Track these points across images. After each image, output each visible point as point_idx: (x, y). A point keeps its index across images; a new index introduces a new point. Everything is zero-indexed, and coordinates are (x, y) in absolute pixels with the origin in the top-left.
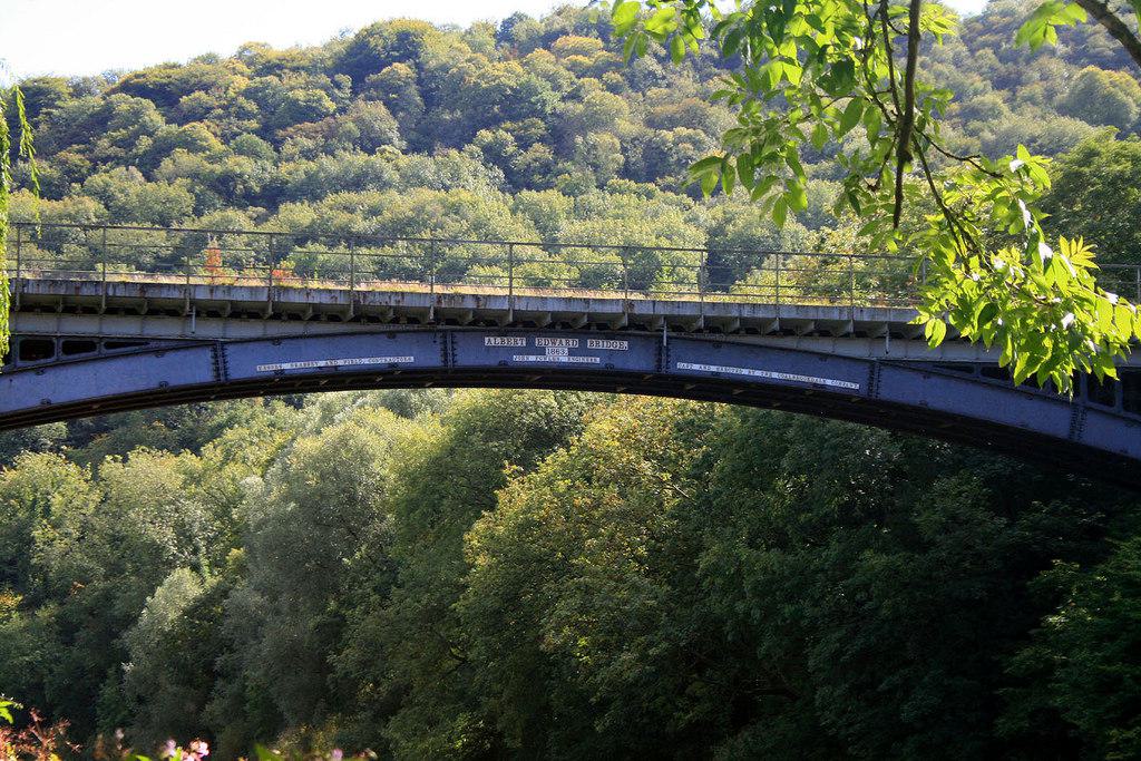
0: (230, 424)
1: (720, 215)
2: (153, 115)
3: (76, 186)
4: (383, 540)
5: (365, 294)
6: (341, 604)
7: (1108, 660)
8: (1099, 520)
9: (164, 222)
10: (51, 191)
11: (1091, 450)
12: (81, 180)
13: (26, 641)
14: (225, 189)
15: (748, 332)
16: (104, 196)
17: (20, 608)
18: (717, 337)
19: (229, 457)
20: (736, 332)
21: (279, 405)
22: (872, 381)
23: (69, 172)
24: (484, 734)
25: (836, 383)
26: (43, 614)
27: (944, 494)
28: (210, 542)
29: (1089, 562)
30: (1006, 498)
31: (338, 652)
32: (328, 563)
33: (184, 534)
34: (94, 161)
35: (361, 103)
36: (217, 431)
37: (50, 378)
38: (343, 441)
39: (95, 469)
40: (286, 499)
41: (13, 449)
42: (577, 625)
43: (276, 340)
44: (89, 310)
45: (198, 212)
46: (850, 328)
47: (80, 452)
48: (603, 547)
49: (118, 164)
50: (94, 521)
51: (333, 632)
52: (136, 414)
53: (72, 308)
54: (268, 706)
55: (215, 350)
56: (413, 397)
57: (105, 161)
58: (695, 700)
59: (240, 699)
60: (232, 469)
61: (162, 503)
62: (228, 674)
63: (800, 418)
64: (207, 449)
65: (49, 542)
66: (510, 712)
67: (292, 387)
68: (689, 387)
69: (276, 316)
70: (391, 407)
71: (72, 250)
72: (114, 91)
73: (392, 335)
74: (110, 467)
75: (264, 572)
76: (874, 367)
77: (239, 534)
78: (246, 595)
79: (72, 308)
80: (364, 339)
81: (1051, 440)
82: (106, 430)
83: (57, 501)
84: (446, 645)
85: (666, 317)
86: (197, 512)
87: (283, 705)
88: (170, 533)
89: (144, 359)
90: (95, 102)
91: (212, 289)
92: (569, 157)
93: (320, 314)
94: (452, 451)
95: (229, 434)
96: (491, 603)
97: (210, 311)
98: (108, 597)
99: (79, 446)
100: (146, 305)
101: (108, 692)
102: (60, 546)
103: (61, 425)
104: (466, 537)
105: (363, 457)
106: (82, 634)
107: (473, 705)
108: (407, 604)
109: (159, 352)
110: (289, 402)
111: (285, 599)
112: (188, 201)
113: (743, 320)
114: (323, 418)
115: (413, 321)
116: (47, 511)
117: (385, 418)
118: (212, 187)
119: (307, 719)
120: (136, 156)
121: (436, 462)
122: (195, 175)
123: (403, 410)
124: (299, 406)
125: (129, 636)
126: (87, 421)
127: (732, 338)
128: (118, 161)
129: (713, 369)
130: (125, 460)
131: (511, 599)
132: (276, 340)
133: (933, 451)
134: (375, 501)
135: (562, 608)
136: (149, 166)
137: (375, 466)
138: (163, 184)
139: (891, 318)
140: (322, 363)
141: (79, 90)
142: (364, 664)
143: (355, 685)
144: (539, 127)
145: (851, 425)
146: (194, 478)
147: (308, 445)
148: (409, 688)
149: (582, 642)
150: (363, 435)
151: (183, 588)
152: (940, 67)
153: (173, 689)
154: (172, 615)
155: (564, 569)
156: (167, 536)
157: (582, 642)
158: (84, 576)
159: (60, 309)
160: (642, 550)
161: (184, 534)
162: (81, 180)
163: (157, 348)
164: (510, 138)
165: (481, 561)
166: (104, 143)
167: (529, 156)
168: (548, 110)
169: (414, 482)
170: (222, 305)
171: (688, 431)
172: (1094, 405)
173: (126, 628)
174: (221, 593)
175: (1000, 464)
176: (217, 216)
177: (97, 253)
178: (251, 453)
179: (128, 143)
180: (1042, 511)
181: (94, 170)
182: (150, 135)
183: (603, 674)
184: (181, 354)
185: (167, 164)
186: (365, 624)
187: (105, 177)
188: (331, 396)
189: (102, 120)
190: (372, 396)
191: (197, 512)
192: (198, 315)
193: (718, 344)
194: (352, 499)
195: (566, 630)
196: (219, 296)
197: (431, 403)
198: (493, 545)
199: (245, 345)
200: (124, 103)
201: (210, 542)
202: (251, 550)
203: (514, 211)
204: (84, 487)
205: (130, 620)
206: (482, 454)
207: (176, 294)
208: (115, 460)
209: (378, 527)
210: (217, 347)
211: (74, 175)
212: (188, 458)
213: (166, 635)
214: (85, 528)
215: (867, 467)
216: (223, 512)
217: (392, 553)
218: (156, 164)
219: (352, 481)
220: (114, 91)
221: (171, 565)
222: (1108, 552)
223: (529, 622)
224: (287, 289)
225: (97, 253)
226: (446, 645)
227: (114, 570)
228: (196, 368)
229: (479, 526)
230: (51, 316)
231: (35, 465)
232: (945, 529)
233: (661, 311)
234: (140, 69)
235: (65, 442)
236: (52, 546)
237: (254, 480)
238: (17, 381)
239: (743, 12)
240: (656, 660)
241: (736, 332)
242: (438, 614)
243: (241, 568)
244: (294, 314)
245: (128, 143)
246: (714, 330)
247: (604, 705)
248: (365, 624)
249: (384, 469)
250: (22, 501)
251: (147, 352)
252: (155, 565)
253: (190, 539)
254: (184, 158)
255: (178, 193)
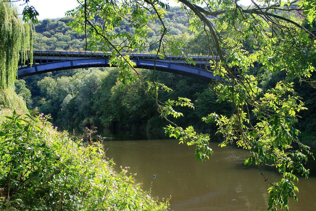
0: (77, 72)
1: (152, 40)
2: (64, 24)
3: (53, 36)
4: (99, 90)
5: (93, 53)
6: (93, 100)
7: (203, 107)
8: (203, 86)
9: (66, 41)
10: (48, 36)
11: (171, 69)
12: (54, 35)
13: (46, 105)
14: (76, 36)
15: (155, 59)
16: (57, 37)
17: (45, 100)
18: (146, 59)
19: (76, 77)
20: (149, 59)
21: (84, 70)
22: (169, 66)
23: (52, 33)
24: (114, 119)
25: (164, 66)
26: (49, 101)
27: (180, 83)
28: (74, 90)
29: (201, 92)
30: (190, 83)
31: (92, 107)
32: (91, 93)
33: (70, 89)
34: (55, 32)
35: (97, 23)
36: (75, 73)
37: (46, 65)
38: (93, 75)
39: (56, 79)
40: (85, 84)
41: (44, 76)
42: (127, 102)
43: (80, 60)
44: (52, 55)
45: (72, 40)
46: (198, 59)
47: (54, 77)
48: (131, 91)
49: (59, 32)
50: (56, 87)
51: (92, 104)
52: (62, 71)
53: (49, 55)
54: (82, 115)
55: (71, 62)
56: (104, 68)
57: (57, 32)
58: (145, 113)
59: (78, 114)
60: (77, 79)
61: (66, 85)
62: (77, 110)
63: (159, 71)
64: (73, 76)
65: (50, 90)
66: (118, 115)
67: (86, 67)
68: (142, 67)
69: (80, 56)
70: (100, 70)
71: (52, 46)
72: (58, 21)
73: (97, 59)
74: (58, 79)
75: (81, 95)
76: (170, 64)
77: (78, 88)
78: (79, 98)
79: (49, 55)
80: (93, 60)
81: (196, 75)
82: (58, 73)
83: (50, 84)
84: (108, 105)
85: (139, 56)
86: (72, 86)
87: (85, 115)
88: (68, 89)
89: (60, 63)
90: (56, 22)
91: (70, 52)
92: (129, 31)
93: (88, 56)
94: (109, 77)
95: (76, 74)
96: (115, 99)
97: (70, 56)
98: (59, 99)
99: (54, 76)
100: (60, 55)
101: (59, 113)
102: (51, 91)
103: (51, 72)
104: (111, 89)
105: (96, 77)
106: (55, 104)
107: (113, 115)
108: (103, 99)
109: (63, 62)
110: (86, 69)
111: (85, 99)
112: (70, 38)
113: (150, 57)
114: (90, 72)
115: (101, 57)
116: (49, 86)
117: (100, 71)
118: (74, 36)
119: (88, 117)
120: (62, 31)
121: (107, 78)
122: (71, 34)
123: (102, 70)
124: (87, 70)
125: (61, 105)
126: (55, 72)
127: (148, 60)
128: (59, 32)
129: (146, 64)
130: (61, 78)
131: (118, 98)
132: (80, 60)
133: (179, 76)
134: (98, 84)
135: (125, 100)
136: (64, 32)
137: (98, 79)
138: (66, 35)
139: (172, 56)
140: (87, 63)
141: (53, 21)
142: (97, 108)
143: (96, 112)
144: (124, 27)
145: (167, 72)
146: (71, 81)
147: (88, 76)
148: (103, 112)
149: (128, 105)
150: (96, 74)
151: (70, 97)
152: (185, 18)
153: (68, 112)
154: (68, 101)
155: (125, 94)
156: (67, 89)
157: (128, 105)
158: (55, 96)
159: (60, 55)
160: (137, 91)
161: (70, 89)
162: (54, 35)
163: (57, 61)
164: (120, 28)
165: (113, 93)
166: (57, 29)
167: (123, 31)
168: (125, 24)
169: (103, 81)
170: (72, 55)
171: (144, 73)
172: (202, 69)
173: (61, 103)
174: (75, 98)
175: (189, 78)
176: (75, 40)
177: (56, 46)
178: (80, 77)
179: (61, 29)
180: (195, 85)
181: (55, 33)
182: (64, 28)
183: (131, 109)
184: (66, 62)
185: (67, 32)
186: (97, 102)
187: (57, 34)
188: (92, 68)
189: (57, 25)
190: (97, 68)
191: (72, 86)
192: (68, 56)
193: (146, 60)
194: (95, 84)
195: (126, 103)
196: (71, 53)
197: (107, 69)
198: (115, 90)
199: (89, 60)
200: (60, 23)
201: (74, 90)
202: (80, 92)
203: (120, 40)
204: (55, 82)
205: (62, 102)
206: (114, 77)
207: (65, 53)
208: (59, 78)
209: (99, 88)
210: (71, 61)
211: (52, 34)
212: (70, 78)
213: (67, 104)
214: (55, 88)
215: (170, 78)
216: (76, 86)
217: (100, 92)
218: (65, 32)
219: (94, 81)
220: (58, 21)
221: (68, 94)
222: (204, 91)
223: (120, 102)
224: (81, 52)
225: (56, 46)
226: (108, 105)
227: (59, 94)
228: (68, 64)
229: (113, 88)
230: (58, 57)
231: (47, 79)
232: (181, 88)
233: (138, 55)
234: (62, 17)
235: (51, 75)
236: (50, 91)
237: (80, 81)
238: (41, 66)
239: (49, 120)
240: (139, 107)
241: (149, 59)
242: (107, 101)
243: (78, 94)
244: (83, 56)
245: (61, 29)
246: (151, 59)
247: (131, 114)
248: (97, 102)
249: (99, 79)
250: (45, 84)
251: (61, 62)
252: (65, 94)
253: (71, 90)
254: (69, 31)
255: (69, 37)
